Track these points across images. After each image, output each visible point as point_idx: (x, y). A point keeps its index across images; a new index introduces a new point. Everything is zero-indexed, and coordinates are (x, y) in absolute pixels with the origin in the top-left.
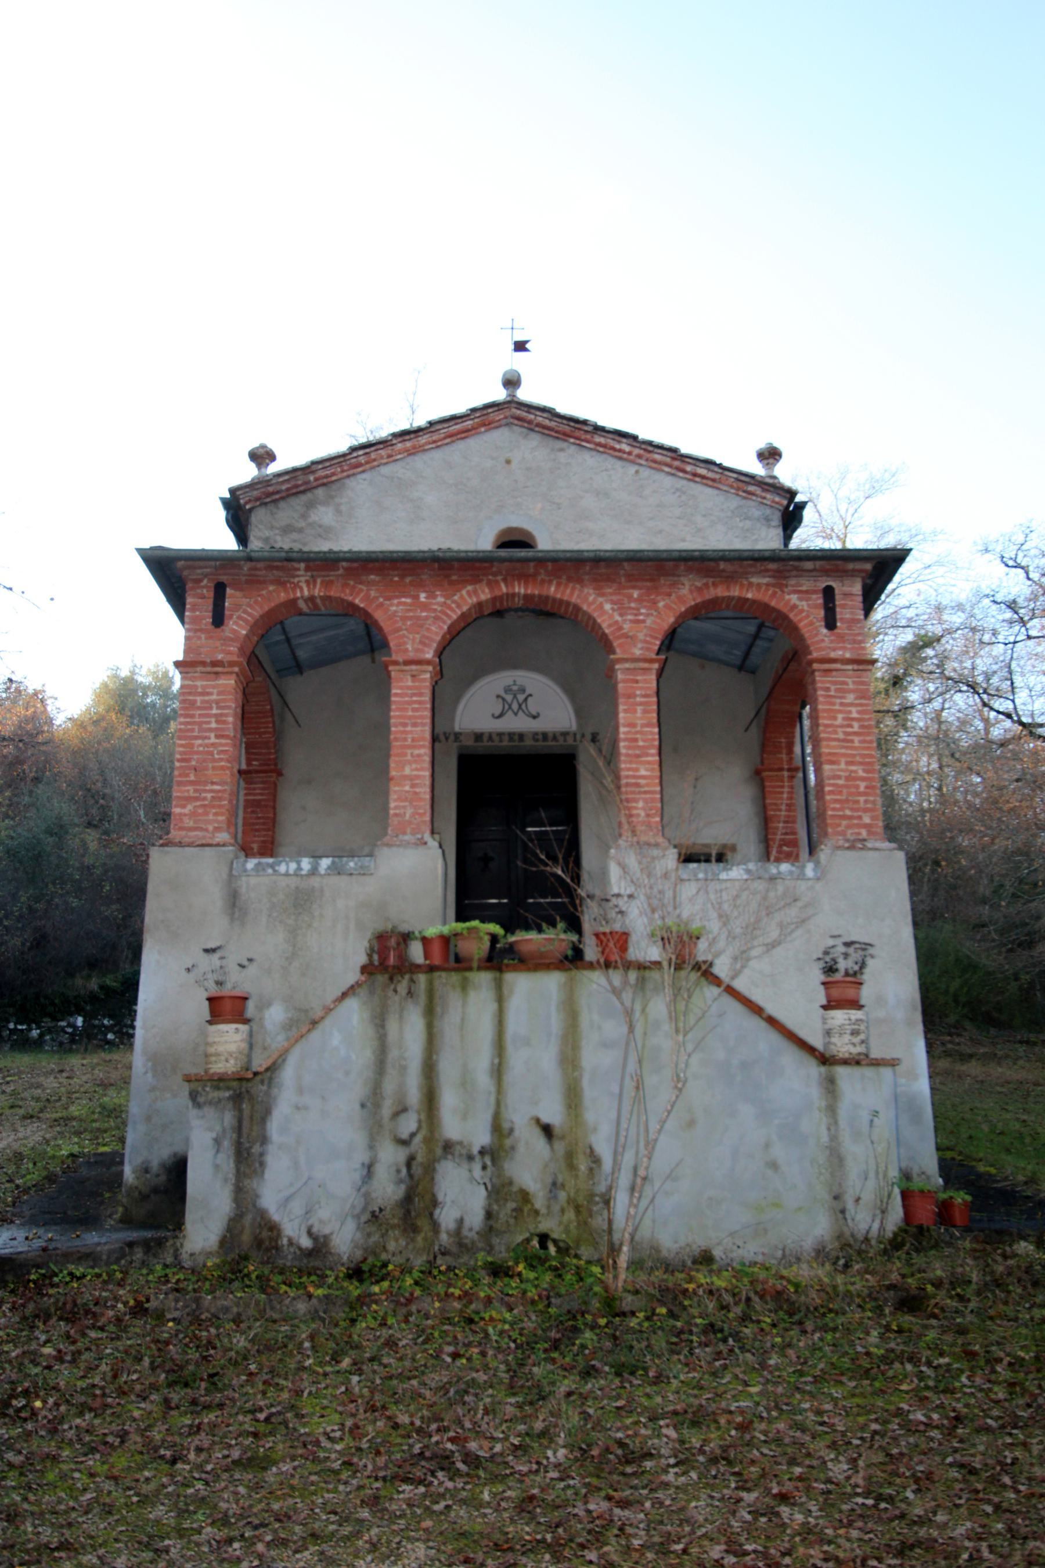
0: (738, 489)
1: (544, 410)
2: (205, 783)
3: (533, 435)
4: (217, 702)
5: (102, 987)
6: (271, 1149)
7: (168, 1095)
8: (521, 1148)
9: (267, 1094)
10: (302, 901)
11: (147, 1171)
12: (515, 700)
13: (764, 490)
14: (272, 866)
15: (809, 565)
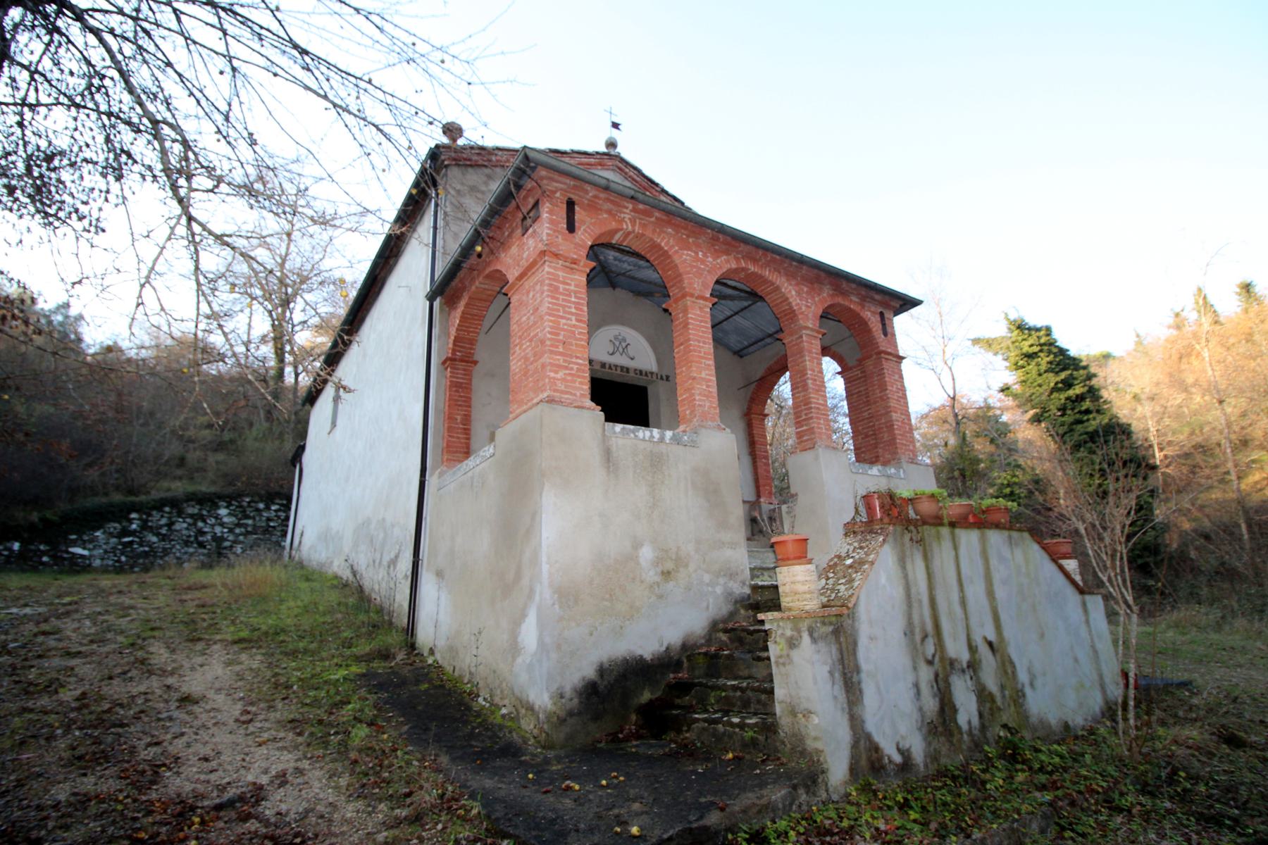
1: (635, 168)
2: (571, 356)
4: (576, 292)
5: (41, 519)
6: (863, 676)
7: (573, 624)
8: (984, 662)
9: (853, 626)
10: (656, 462)
11: (562, 697)
12: (620, 345)
14: (633, 432)
15: (877, 297)
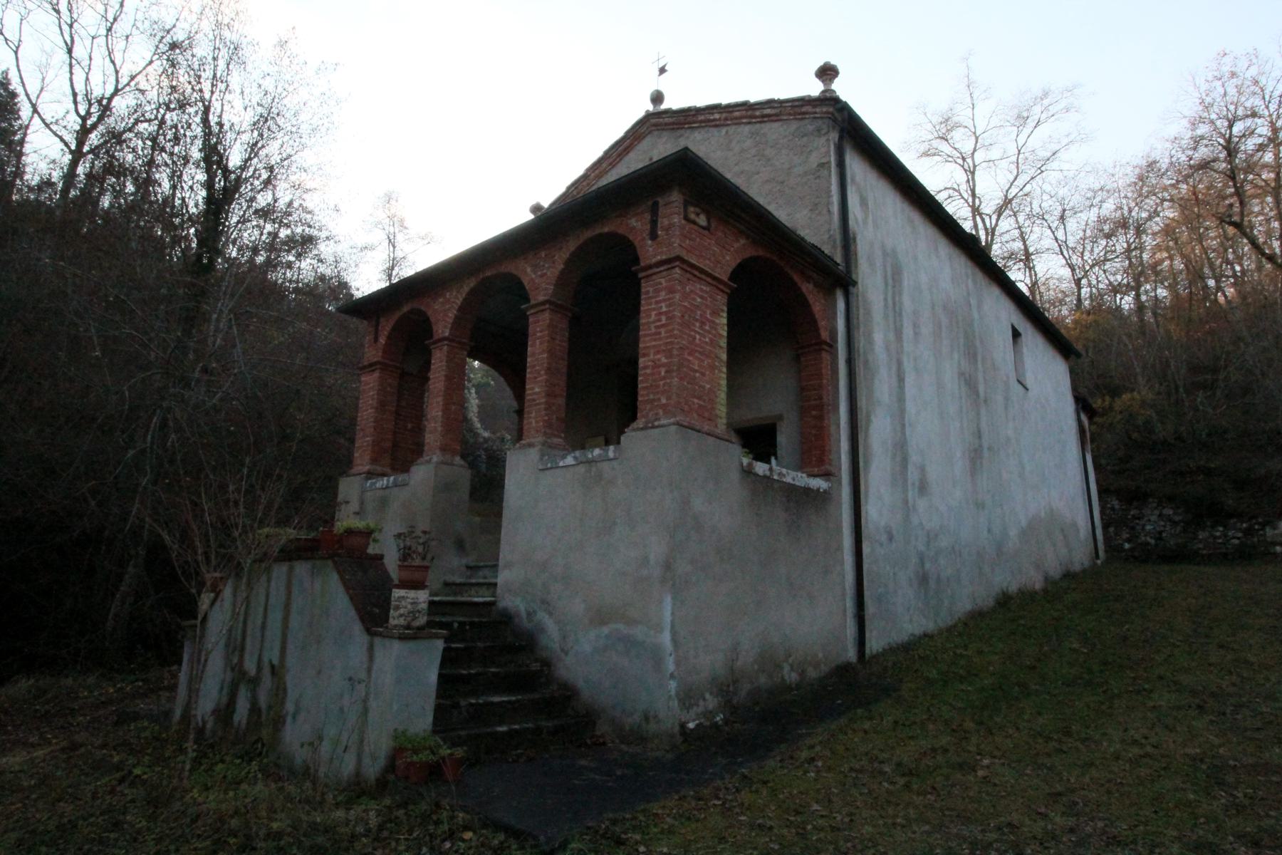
0: (795, 114)
3: (665, 133)
13: (815, 106)
